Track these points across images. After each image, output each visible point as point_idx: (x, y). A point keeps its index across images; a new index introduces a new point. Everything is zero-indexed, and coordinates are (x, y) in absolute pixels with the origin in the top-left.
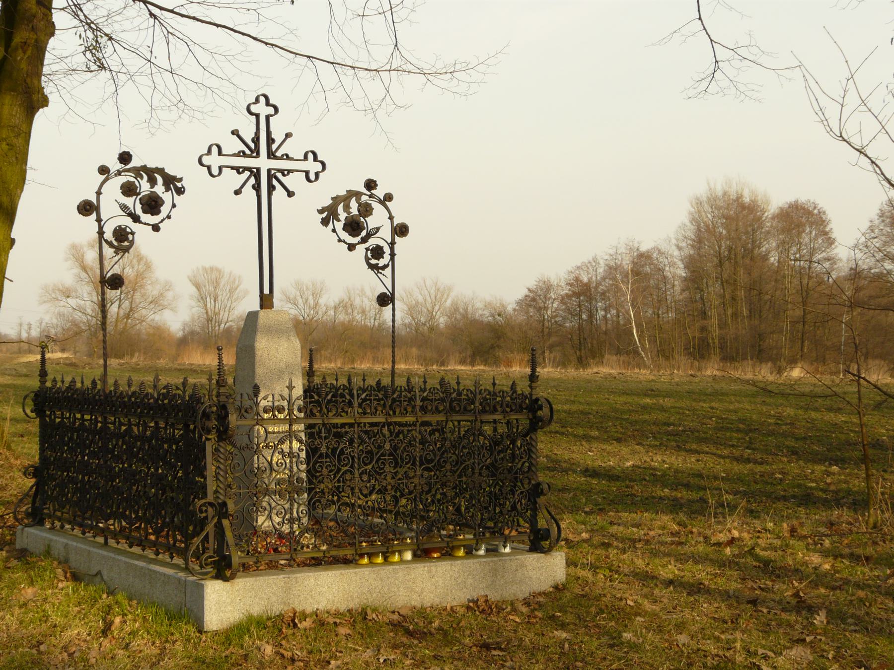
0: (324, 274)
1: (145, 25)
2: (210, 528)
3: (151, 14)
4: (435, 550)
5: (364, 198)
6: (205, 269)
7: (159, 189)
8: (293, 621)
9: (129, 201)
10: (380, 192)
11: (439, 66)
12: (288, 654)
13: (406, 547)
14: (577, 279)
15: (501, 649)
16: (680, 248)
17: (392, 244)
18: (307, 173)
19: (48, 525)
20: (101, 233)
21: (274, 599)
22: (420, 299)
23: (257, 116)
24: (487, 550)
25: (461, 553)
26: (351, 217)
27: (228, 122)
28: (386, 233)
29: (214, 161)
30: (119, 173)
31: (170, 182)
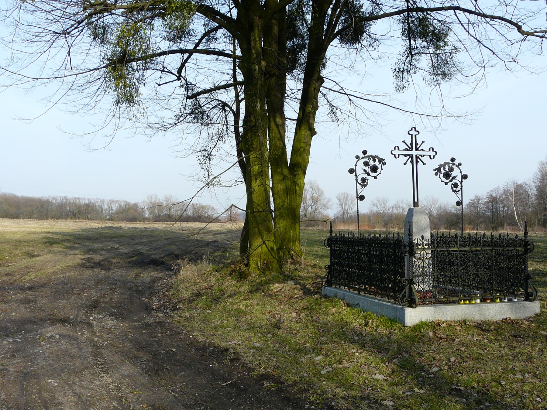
0: (438, 196)
1: (347, 104)
2: (407, 289)
3: (350, 100)
4: (488, 299)
5: (451, 165)
6: (342, 193)
7: (377, 163)
8: (439, 323)
9: (366, 168)
10: (456, 163)
11: (460, 114)
12: (439, 336)
13: (477, 298)
14: (491, 195)
15: (521, 338)
16: (535, 183)
17: (461, 182)
18: (430, 156)
19: (334, 287)
20: (357, 180)
21: (430, 315)
22: (426, 204)
23: (412, 135)
24: (508, 300)
25: (498, 300)
26: (446, 172)
27: (401, 137)
28: (459, 178)
29: (396, 152)
30: (363, 158)
31: (381, 161)
